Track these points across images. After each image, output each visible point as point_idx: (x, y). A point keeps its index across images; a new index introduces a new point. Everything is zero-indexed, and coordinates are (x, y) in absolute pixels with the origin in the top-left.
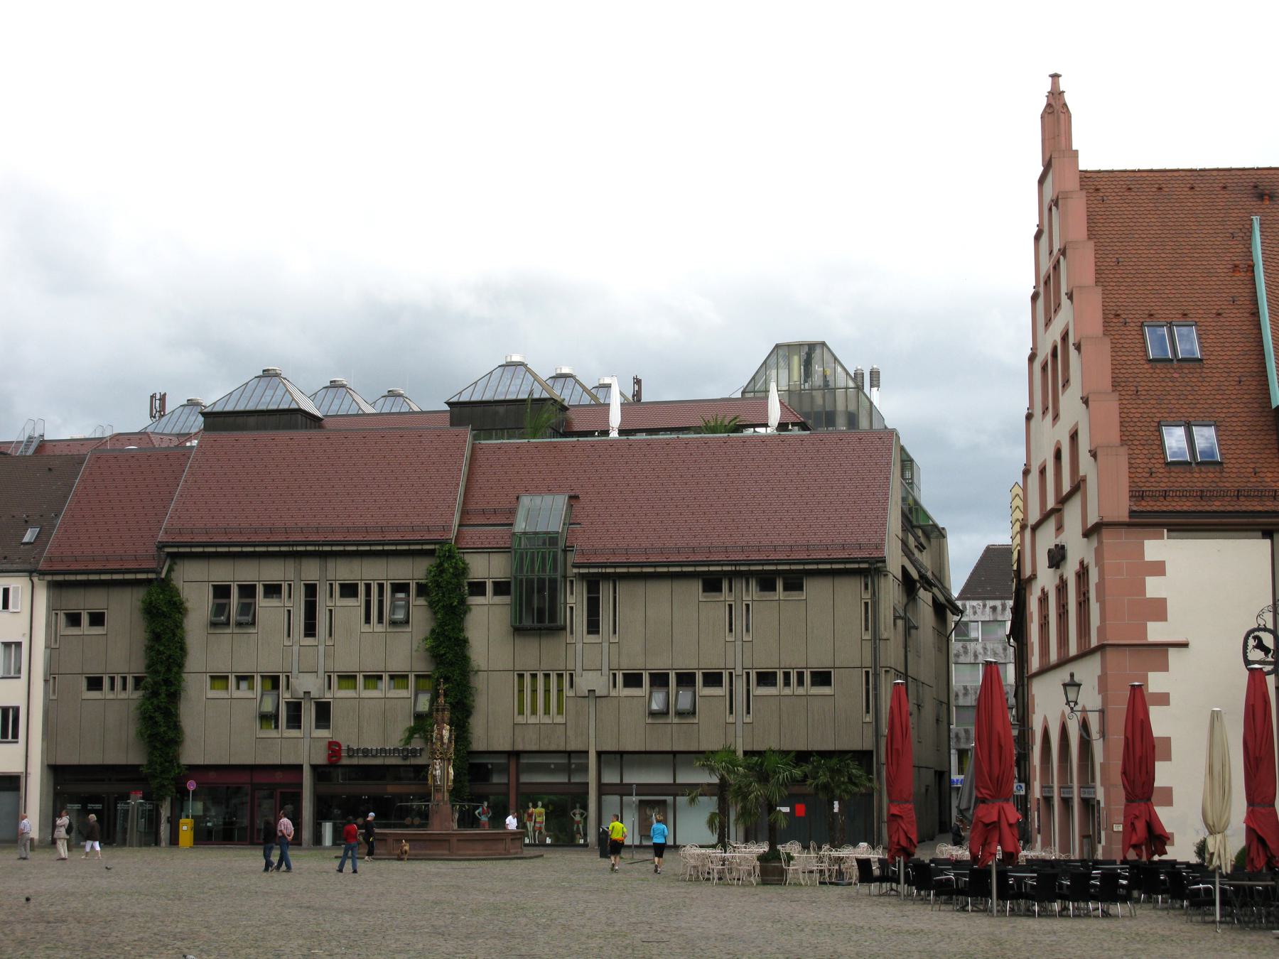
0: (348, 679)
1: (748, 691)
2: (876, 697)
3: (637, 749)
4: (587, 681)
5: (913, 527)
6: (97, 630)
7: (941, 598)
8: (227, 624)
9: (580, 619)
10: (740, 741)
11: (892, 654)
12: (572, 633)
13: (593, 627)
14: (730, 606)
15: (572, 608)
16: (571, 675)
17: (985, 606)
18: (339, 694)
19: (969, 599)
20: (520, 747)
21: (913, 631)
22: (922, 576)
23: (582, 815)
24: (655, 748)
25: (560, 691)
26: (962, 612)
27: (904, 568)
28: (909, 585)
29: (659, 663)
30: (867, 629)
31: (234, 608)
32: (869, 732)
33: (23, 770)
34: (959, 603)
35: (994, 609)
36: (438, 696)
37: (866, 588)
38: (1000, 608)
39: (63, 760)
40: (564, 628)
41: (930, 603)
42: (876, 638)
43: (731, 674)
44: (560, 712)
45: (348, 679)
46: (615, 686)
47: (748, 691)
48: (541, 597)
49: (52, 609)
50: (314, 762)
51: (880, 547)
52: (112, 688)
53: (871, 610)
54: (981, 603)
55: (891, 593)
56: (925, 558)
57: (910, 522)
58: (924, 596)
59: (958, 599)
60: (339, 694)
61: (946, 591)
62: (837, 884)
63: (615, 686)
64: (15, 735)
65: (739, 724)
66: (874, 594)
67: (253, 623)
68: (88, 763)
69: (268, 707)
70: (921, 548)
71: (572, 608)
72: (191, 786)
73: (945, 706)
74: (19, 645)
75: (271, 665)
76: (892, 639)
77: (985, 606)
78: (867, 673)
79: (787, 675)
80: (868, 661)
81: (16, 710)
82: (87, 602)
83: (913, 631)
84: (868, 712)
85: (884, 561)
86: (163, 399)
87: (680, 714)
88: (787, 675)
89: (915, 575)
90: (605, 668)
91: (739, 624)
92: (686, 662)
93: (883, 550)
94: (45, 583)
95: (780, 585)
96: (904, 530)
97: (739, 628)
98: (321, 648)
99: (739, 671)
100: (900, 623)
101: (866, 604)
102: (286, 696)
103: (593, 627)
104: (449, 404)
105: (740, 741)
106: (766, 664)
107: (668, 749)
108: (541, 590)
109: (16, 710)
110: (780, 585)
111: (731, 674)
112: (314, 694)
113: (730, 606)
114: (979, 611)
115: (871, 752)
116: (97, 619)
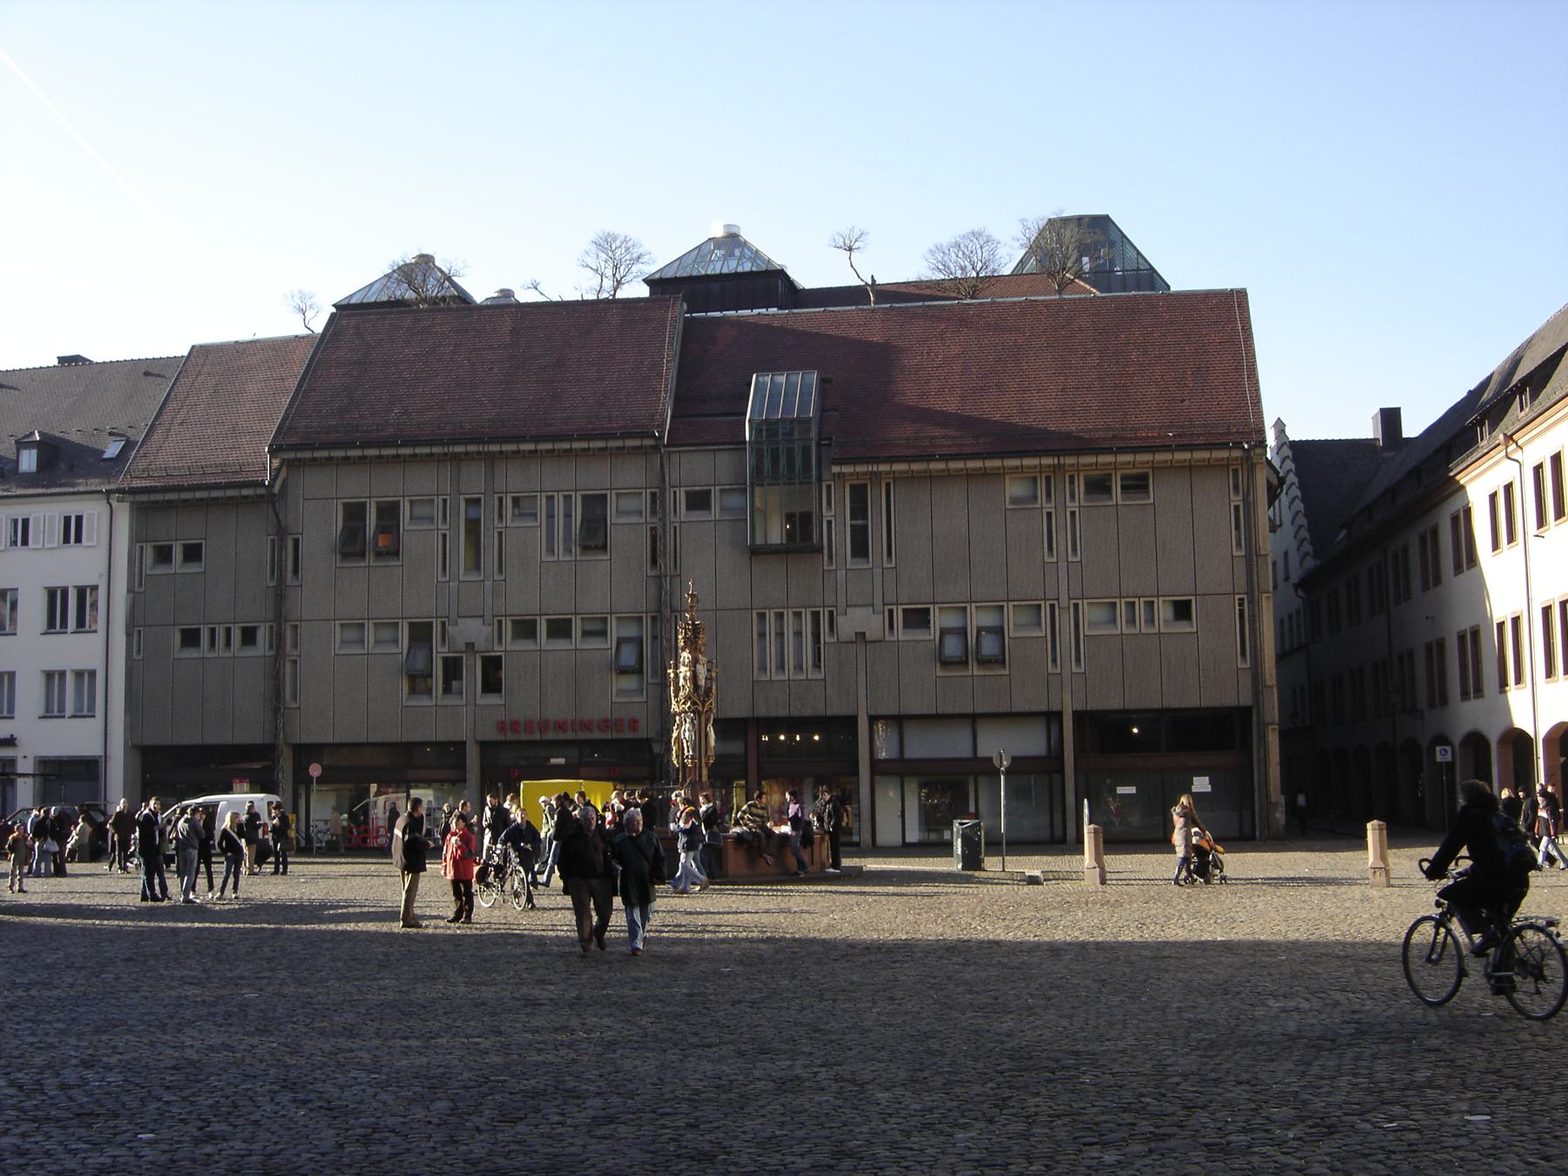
0: (525, 629)
2: (1253, 631)
3: (924, 712)
4: (854, 621)
6: (193, 568)
8: (362, 555)
9: (843, 540)
10: (1067, 697)
12: (830, 557)
13: (860, 547)
14: (1049, 514)
15: (829, 523)
18: (510, 647)
23: (249, 826)
30: (1239, 544)
31: (368, 537)
32: (1246, 680)
33: (101, 753)
39: (152, 739)
40: (821, 550)
44: (817, 664)
45: (525, 629)
46: (891, 627)
49: (136, 538)
50: (480, 739)
52: (212, 643)
60: (510, 647)
62: (968, 880)
63: (891, 627)
65: (1067, 673)
67: (395, 553)
68: (185, 742)
69: (420, 664)
71: (829, 523)
72: (315, 770)
75: (422, 606)
87: (984, 662)
90: (878, 603)
91: (1062, 540)
94: (126, 505)
97: (1062, 548)
98: (488, 584)
99: (1064, 601)
101: (1237, 508)
102: (440, 652)
103: (860, 547)
105: (1067, 697)
109: (92, 674)
112: (480, 645)
113: (1049, 514)
116: (193, 553)
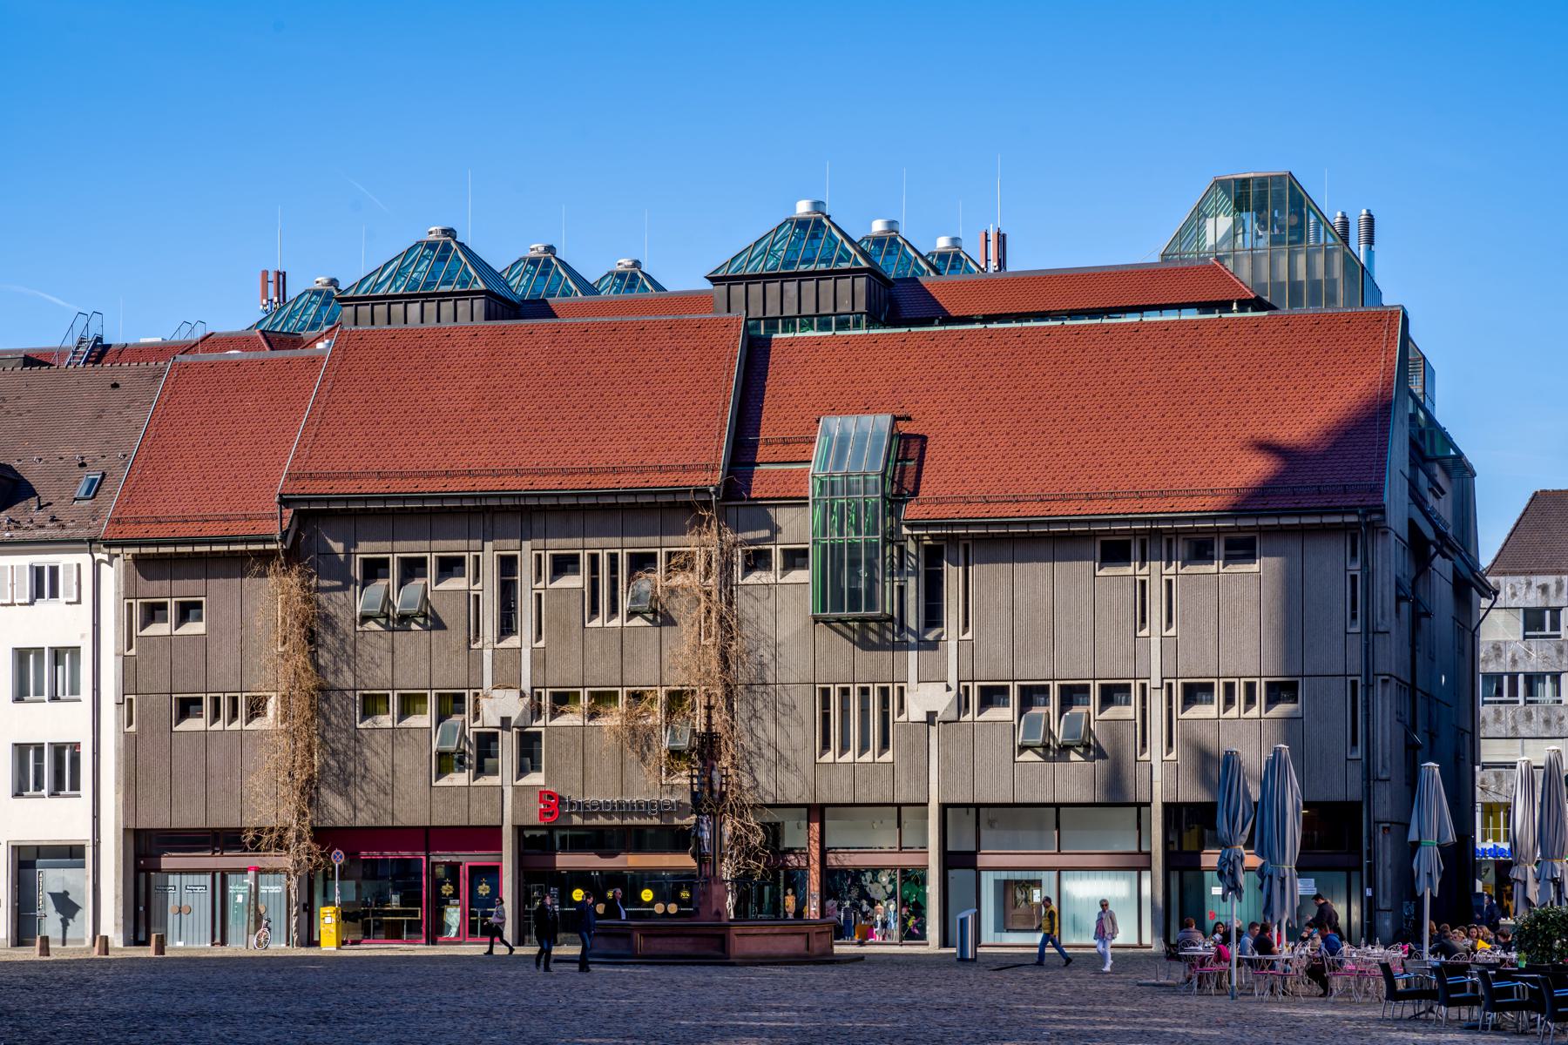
1: (1170, 711)
5: (1426, 460)
7: (1465, 572)
11: (1391, 655)
16: (901, 689)
17: (1529, 584)
19: (1504, 574)
20: (823, 798)
21: (1424, 620)
22: (1441, 535)
24: (1027, 800)
25: (885, 717)
26: (1496, 593)
27: (1412, 523)
28: (1419, 548)
29: (1033, 670)
32: (1356, 773)
34: (1491, 580)
35: (1544, 589)
36: (585, 816)
37: (1354, 554)
38: (1553, 589)
39: (143, 824)
41: (1450, 578)
42: (1370, 632)
43: (1144, 686)
47: (1170, 711)
48: (854, 575)
49: (129, 593)
51: (1377, 490)
53: (1360, 592)
54: (1522, 579)
55: (1390, 560)
56: (1443, 507)
57: (1421, 452)
58: (1442, 566)
59: (1490, 570)
61: (1473, 566)
64: (75, 786)
66: (1365, 562)
70: (1438, 491)
73: (1467, 737)
74: (75, 651)
76: (1393, 632)
77: (1529, 584)
78: (1354, 683)
79: (1229, 688)
80: (1356, 665)
81: (75, 746)
82: (172, 591)
83: (1424, 620)
84: (1354, 743)
85: (1383, 512)
86: (281, 277)
88: (1229, 688)
89: (1429, 533)
92: (1074, 669)
93: (1381, 494)
95: (1220, 548)
96: (1414, 465)
100: (1405, 606)
101: (1354, 578)
104: (714, 280)
105: (1157, 787)
106: (1197, 671)
107: (1048, 799)
108: (855, 563)
110: (1220, 548)
111: (1144, 686)
114: (1521, 594)
115: (1358, 805)
